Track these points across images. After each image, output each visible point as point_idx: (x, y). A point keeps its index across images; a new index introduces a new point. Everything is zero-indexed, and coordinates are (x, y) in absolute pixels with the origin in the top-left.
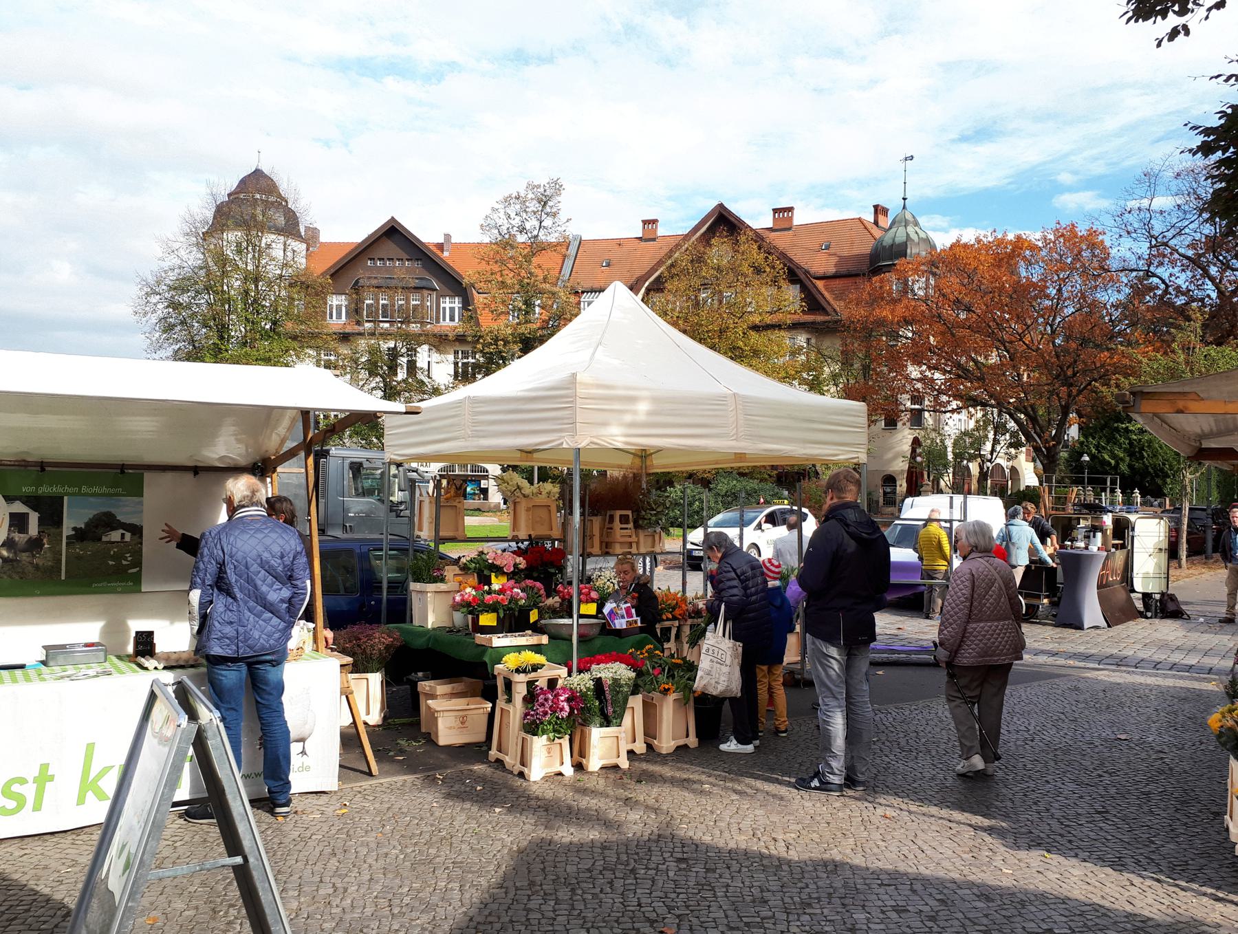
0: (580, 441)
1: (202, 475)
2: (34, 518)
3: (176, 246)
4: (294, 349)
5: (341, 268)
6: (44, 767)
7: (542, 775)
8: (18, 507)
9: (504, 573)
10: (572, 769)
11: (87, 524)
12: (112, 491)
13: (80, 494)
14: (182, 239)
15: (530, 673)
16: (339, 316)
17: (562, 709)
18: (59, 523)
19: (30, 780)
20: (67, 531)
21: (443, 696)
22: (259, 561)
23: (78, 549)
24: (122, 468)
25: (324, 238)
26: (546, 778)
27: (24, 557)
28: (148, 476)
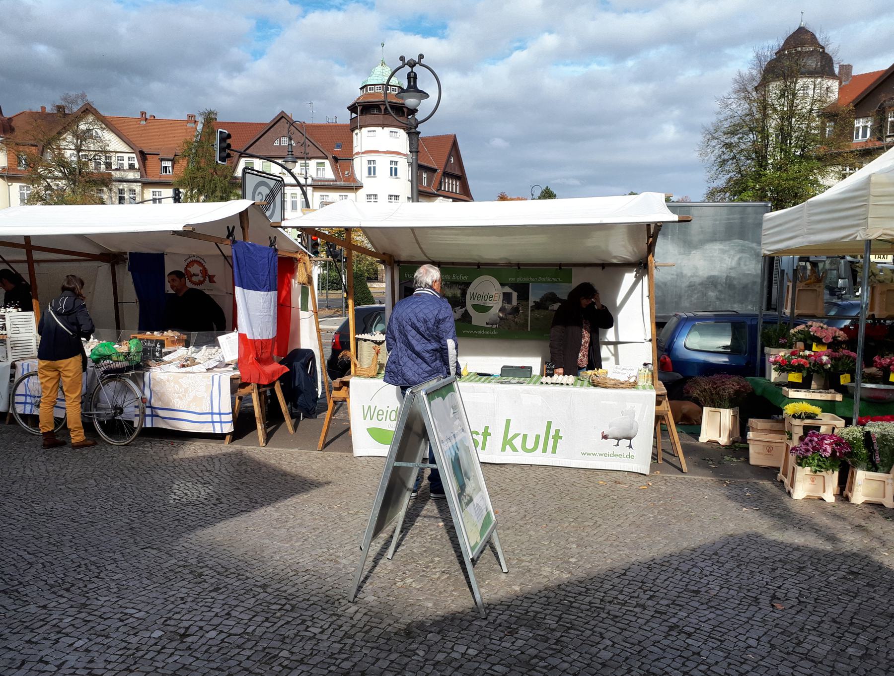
0: (870, 234)
1: (607, 268)
2: (515, 295)
3: (730, 101)
4: (818, 168)
5: (868, 95)
6: (487, 428)
7: (804, 496)
8: (507, 290)
9: (824, 344)
10: (834, 498)
11: (541, 300)
12: (555, 280)
13: (537, 282)
14: (734, 96)
15: (803, 419)
16: (864, 135)
17: (825, 450)
18: (527, 299)
19: (481, 433)
20: (531, 303)
21: (764, 430)
22: (410, 323)
23: (537, 314)
24: (560, 265)
25: (855, 72)
26: (808, 499)
27: (510, 317)
28: (575, 270)
